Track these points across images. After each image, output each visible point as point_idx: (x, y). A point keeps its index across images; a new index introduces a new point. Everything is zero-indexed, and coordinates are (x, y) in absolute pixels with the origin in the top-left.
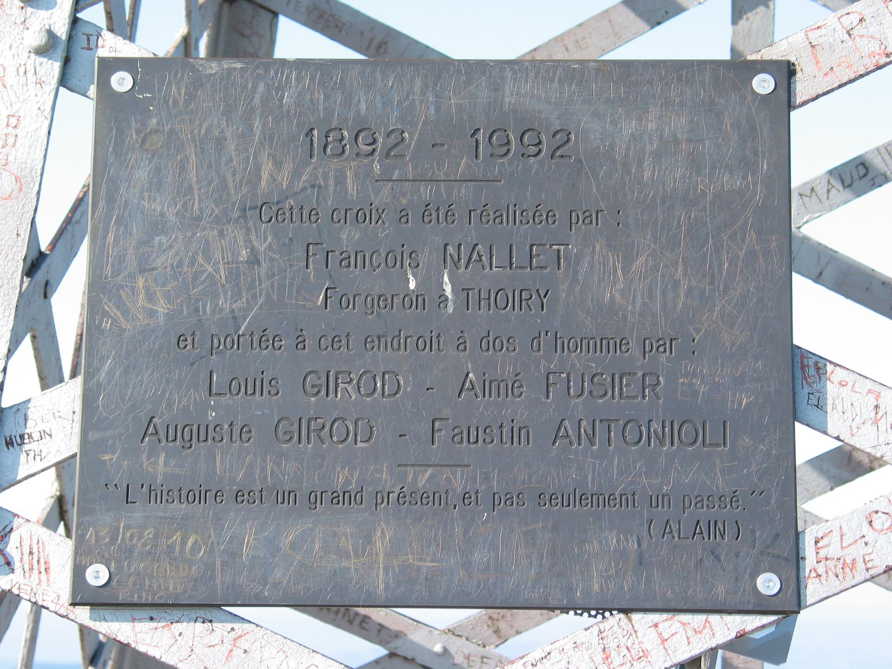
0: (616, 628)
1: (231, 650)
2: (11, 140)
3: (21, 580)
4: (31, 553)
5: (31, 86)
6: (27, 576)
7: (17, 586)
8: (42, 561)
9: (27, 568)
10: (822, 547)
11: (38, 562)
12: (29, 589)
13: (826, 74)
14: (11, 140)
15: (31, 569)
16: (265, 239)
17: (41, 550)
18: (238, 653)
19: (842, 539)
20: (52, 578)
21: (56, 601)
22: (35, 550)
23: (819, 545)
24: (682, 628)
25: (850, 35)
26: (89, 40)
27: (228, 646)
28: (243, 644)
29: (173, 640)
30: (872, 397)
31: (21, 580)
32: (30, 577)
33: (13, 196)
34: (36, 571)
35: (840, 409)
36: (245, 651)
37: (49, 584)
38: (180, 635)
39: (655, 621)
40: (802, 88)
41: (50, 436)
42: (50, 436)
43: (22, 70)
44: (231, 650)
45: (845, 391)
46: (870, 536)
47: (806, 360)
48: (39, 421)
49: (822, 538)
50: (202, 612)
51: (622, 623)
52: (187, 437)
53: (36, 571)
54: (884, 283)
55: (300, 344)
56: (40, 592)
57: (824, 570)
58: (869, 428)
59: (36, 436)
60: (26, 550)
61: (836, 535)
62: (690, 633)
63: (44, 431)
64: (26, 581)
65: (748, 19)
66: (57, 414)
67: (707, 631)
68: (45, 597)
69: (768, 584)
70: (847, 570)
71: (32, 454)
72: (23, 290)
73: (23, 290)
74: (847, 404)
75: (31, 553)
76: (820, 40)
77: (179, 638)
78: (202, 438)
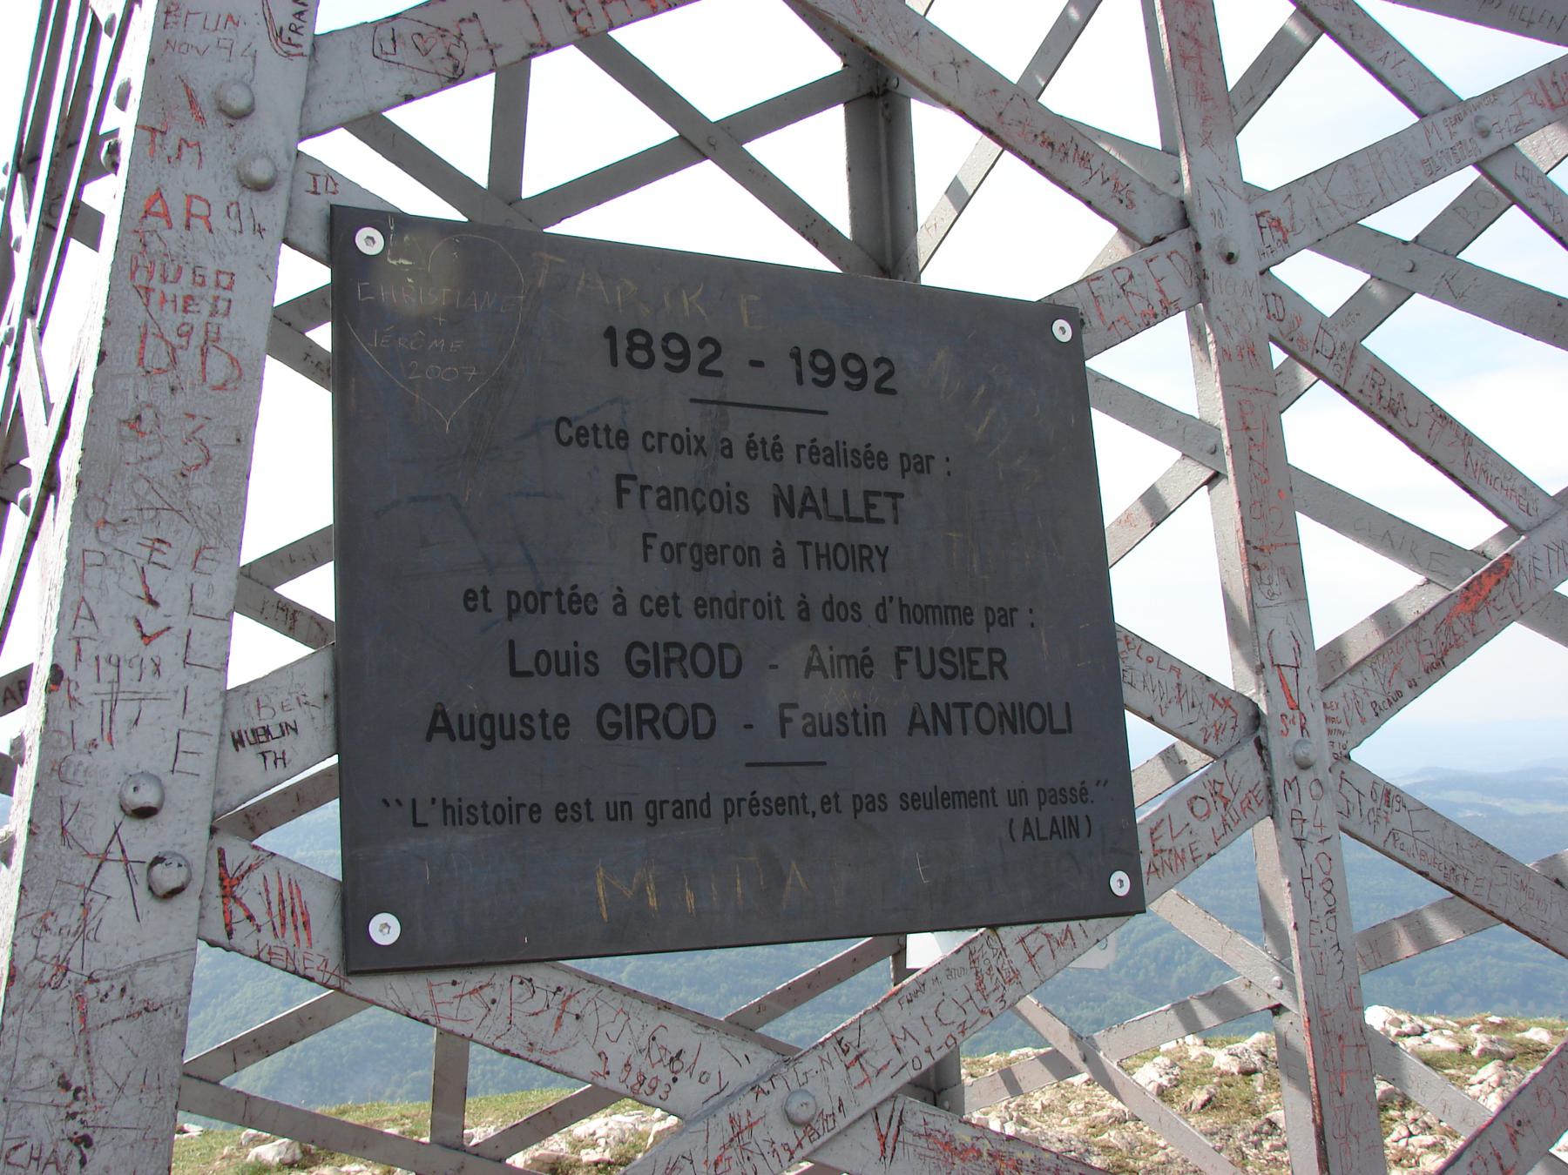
1: (560, 1017)
2: (222, 305)
5: (248, 232)
8: (298, 910)
9: (278, 925)
14: (222, 305)
15: (283, 925)
18: (568, 1020)
27: (554, 1012)
28: (574, 1007)
29: (484, 1011)
30: (1174, 674)
31: (272, 942)
33: (230, 386)
36: (578, 1017)
38: (494, 1002)
42: (295, 730)
43: (233, 209)
44: (560, 1017)
46: (1194, 823)
53: (290, 926)
55: (620, 606)
56: (299, 956)
58: (1174, 707)
59: (275, 732)
60: (274, 897)
62: (1055, 945)
64: (277, 942)
66: (303, 699)
67: (1069, 941)
71: (270, 758)
72: (572, 227)
73: (572, 227)
74: (1155, 682)
75: (282, 901)
76: (1102, 292)
77: (493, 1007)
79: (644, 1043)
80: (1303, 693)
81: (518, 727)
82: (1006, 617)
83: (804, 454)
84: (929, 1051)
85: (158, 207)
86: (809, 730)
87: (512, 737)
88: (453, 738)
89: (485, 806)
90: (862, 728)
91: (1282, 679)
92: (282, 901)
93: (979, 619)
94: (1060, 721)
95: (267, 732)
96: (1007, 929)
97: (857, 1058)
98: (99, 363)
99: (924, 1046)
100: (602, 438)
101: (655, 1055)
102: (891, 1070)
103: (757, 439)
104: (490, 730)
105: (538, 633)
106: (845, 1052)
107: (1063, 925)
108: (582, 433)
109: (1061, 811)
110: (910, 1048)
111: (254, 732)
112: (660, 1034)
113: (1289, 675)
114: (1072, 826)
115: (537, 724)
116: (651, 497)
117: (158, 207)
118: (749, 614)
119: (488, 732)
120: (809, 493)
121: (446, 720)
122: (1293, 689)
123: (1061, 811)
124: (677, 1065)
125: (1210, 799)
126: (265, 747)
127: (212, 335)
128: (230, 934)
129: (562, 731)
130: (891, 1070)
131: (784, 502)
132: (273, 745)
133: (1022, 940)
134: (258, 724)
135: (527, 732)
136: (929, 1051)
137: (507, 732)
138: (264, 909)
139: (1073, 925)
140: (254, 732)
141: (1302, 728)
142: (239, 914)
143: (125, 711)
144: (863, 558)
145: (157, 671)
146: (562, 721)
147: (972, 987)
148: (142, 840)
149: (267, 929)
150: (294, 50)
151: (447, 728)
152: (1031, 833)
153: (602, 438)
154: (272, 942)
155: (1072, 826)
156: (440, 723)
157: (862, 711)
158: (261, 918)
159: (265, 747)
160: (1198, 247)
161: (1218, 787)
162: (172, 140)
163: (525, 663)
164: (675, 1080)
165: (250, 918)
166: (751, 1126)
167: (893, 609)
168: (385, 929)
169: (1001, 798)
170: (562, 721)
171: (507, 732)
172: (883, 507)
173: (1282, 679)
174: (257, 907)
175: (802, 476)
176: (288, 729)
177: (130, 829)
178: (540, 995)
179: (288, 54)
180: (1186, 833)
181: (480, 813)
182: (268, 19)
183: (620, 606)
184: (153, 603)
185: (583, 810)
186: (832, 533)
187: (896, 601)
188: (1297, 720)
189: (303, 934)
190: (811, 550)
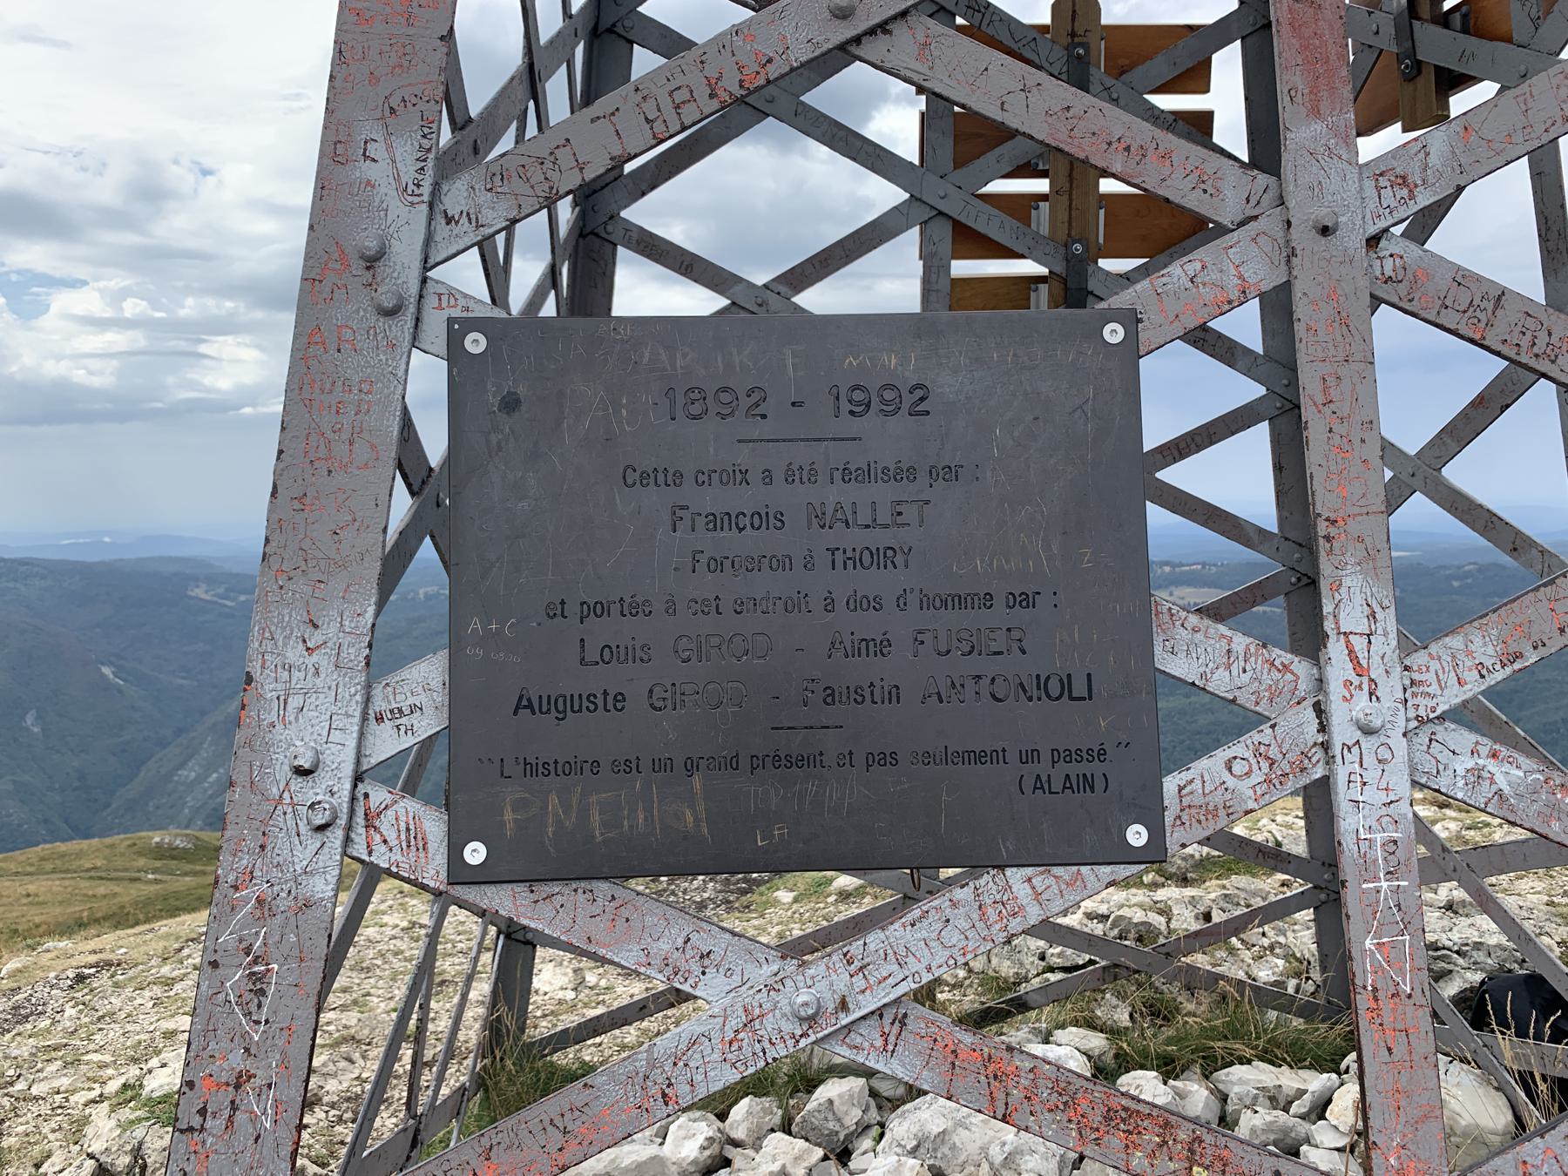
18: (620, 922)
28: (625, 912)
31: (399, 858)
60: (403, 826)
62: (1063, 886)
71: (403, 728)
75: (408, 830)
79: (680, 941)
80: (1376, 660)
81: (585, 703)
82: (1026, 600)
83: (838, 475)
84: (929, 969)
85: (317, 338)
86: (829, 700)
87: (580, 711)
88: (534, 713)
89: (556, 762)
90: (877, 698)
91: (1351, 652)
92: (408, 830)
93: (1000, 602)
94: (1079, 689)
95: (400, 710)
96: (1014, 870)
97: (861, 969)
98: (278, 458)
99: (925, 963)
100: (661, 477)
101: (689, 953)
102: (891, 981)
103: (795, 467)
104: (562, 706)
105: (601, 631)
106: (850, 963)
107: (1075, 868)
108: (644, 476)
109: (1074, 769)
110: (913, 965)
111: (392, 711)
112: (694, 937)
113: (1359, 644)
114: (1088, 783)
115: (600, 702)
116: (701, 521)
117: (317, 338)
118: (765, 567)
119: (561, 708)
120: (839, 507)
121: (529, 700)
122: (1362, 656)
123: (1074, 769)
124: (706, 962)
125: (1253, 761)
126: (399, 722)
127: (357, 430)
128: (370, 853)
129: (619, 706)
130: (891, 981)
131: (819, 518)
132: (404, 720)
133: (1029, 880)
134: (394, 705)
135: (592, 707)
136: (929, 969)
137: (576, 708)
138: (395, 835)
139: (1084, 869)
140: (392, 711)
141: (1371, 694)
142: (377, 838)
143: (294, 702)
144: (884, 557)
145: (317, 673)
146: (620, 697)
147: (975, 916)
148: (308, 791)
149: (396, 850)
150: (416, 199)
151: (530, 706)
152: (1042, 787)
153: (661, 477)
154: (399, 858)
155: (1088, 783)
156: (524, 702)
157: (877, 683)
158: (393, 842)
159: (399, 722)
160: (1289, 223)
161: (1262, 749)
162: (326, 286)
163: (592, 654)
164: (704, 973)
165: (385, 841)
166: (761, 1016)
167: (913, 599)
168: (475, 853)
169: (1012, 756)
170: (620, 697)
171: (576, 708)
172: (910, 513)
173: (1351, 652)
174: (391, 836)
175: (834, 494)
176: (414, 708)
177: (297, 783)
178: (600, 902)
179: (412, 204)
180: (1220, 791)
181: (552, 768)
182: (397, 179)
183: (671, 609)
184: (316, 626)
185: (633, 766)
186: (855, 539)
187: (917, 592)
188: (1365, 687)
189: (422, 855)
190: (839, 556)
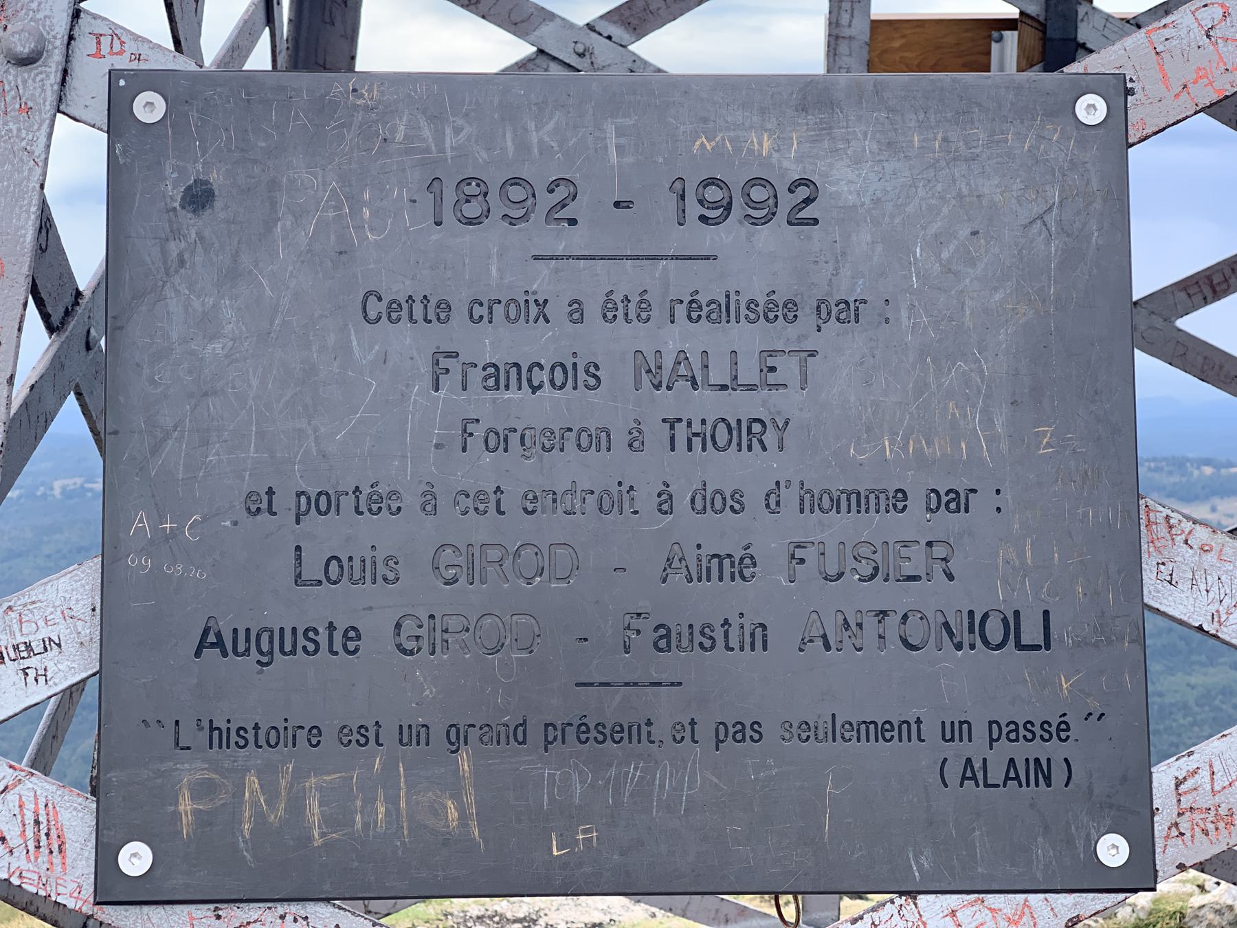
0: (896, 917)
3: (24, 864)
4: (37, 822)
6: (32, 858)
7: (18, 873)
8: (53, 833)
10: (1185, 793)
11: (47, 835)
12: (35, 877)
13: (1177, 96)
16: (371, 348)
17: (51, 818)
19: (1213, 779)
20: (68, 861)
21: (76, 894)
22: (42, 819)
23: (1183, 788)
24: (990, 915)
25: (1208, 36)
26: (99, 43)
31: (24, 864)
32: (36, 858)
34: (44, 850)
35: (1203, 587)
37: (64, 869)
39: (954, 906)
40: (1140, 114)
41: (59, 645)
42: (59, 645)
45: (1210, 558)
47: (1151, 515)
48: (41, 623)
49: (1185, 778)
50: (299, 907)
51: (904, 912)
52: (265, 648)
53: (44, 850)
54: (671, 910)
57: (1188, 825)
60: (29, 818)
61: (1204, 774)
63: (50, 639)
65: (654, 915)
68: (61, 890)
69: (1113, 850)
70: (1221, 825)
71: (32, 673)
75: (37, 822)
78: (288, 648)
